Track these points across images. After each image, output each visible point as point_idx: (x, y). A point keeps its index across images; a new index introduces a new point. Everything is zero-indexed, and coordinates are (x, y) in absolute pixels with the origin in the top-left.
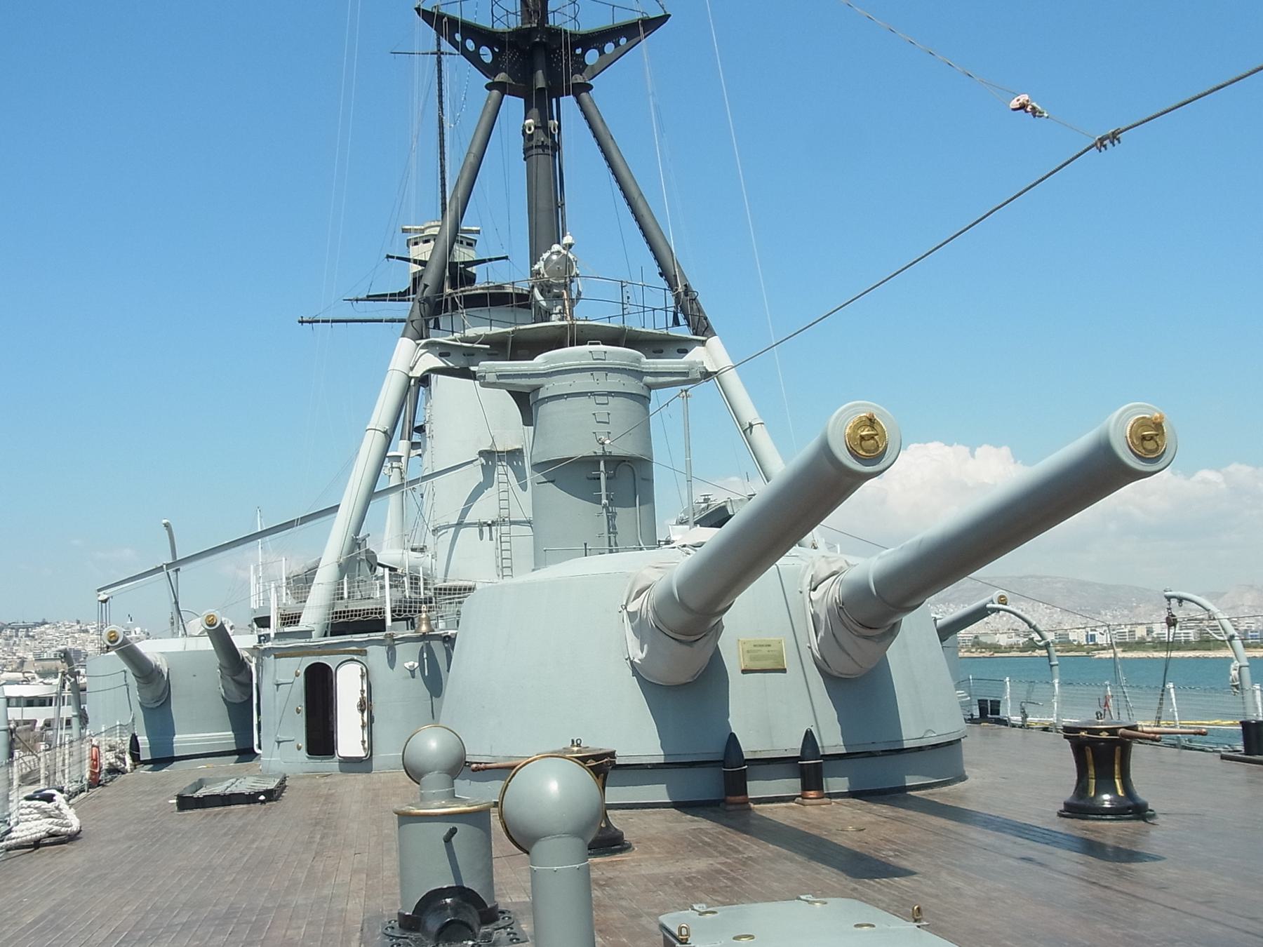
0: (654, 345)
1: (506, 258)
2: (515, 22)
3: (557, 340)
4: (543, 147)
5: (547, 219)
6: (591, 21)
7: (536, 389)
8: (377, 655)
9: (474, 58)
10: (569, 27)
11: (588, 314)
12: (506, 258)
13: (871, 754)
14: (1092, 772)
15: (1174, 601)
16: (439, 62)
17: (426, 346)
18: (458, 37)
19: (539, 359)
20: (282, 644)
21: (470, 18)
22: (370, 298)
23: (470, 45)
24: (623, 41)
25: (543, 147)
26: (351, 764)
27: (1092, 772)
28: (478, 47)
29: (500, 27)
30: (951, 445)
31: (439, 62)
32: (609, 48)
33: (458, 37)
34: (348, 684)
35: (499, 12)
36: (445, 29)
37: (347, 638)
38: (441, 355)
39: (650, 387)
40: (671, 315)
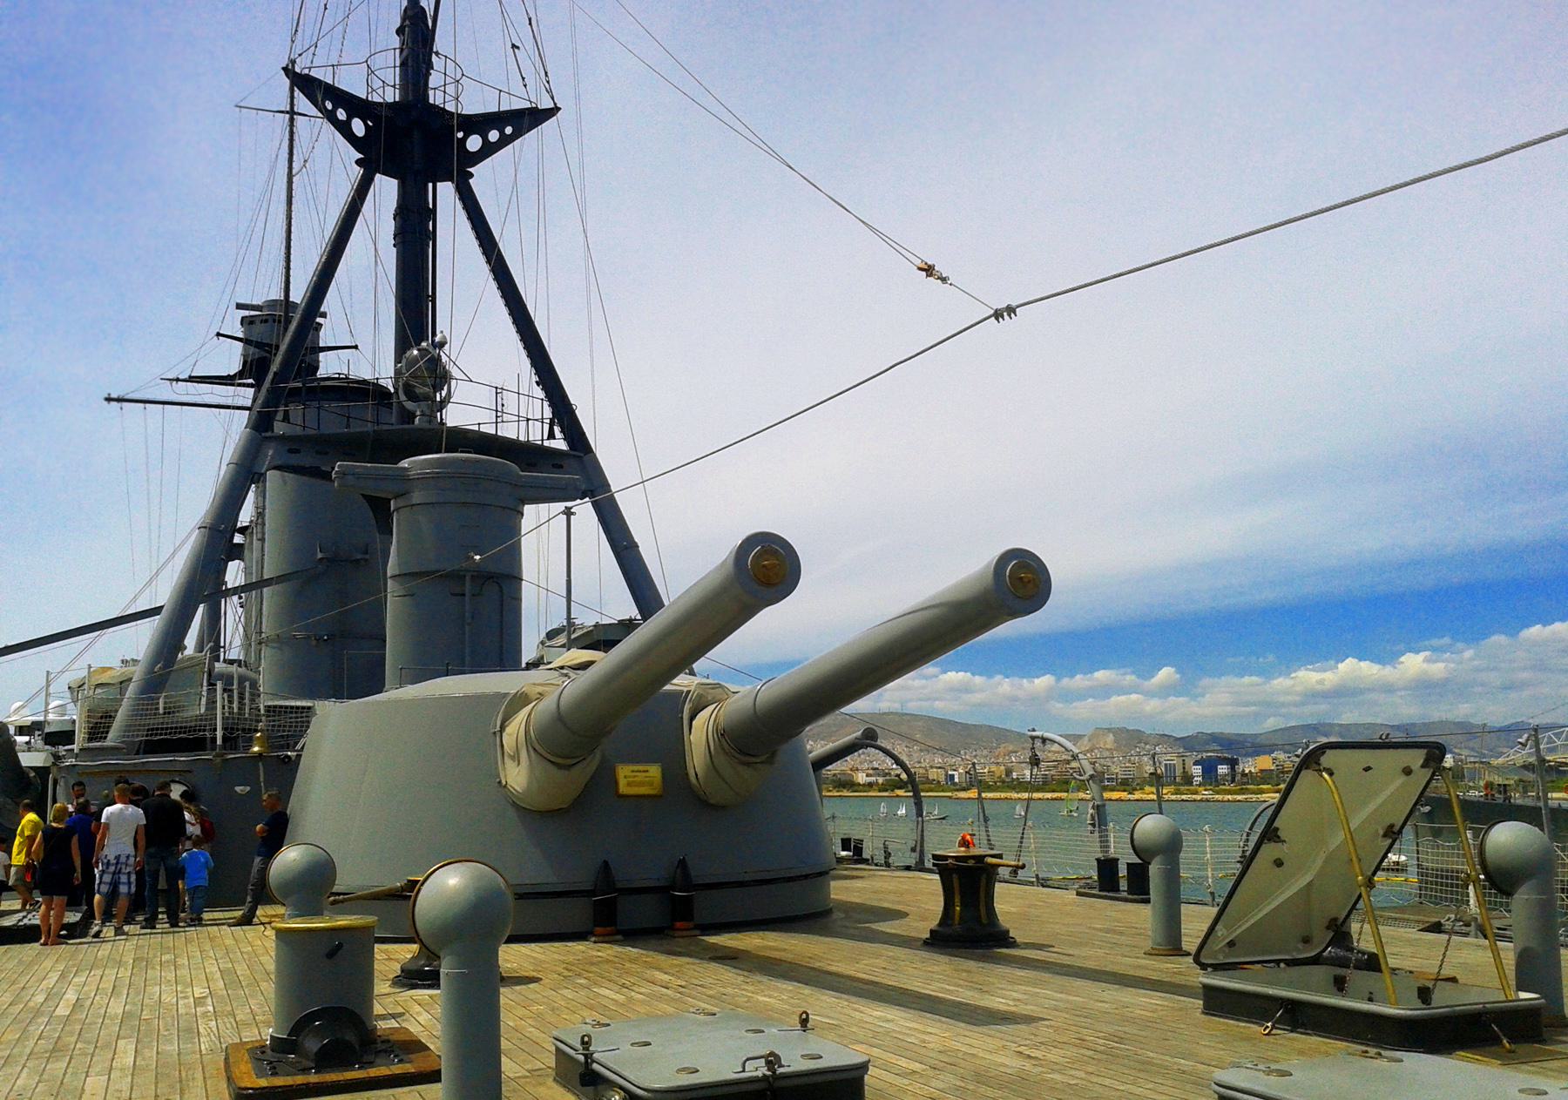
1: (356, 347)
2: (392, 95)
6: (473, 104)
9: (344, 129)
10: (450, 107)
12: (356, 347)
13: (741, 884)
14: (957, 900)
15: (1038, 744)
16: (292, 120)
18: (329, 106)
22: (192, 379)
23: (341, 115)
24: (509, 130)
27: (957, 900)
28: (350, 118)
30: (1262, 771)
31: (292, 120)
32: (494, 136)
35: (377, 84)
40: (546, 427)
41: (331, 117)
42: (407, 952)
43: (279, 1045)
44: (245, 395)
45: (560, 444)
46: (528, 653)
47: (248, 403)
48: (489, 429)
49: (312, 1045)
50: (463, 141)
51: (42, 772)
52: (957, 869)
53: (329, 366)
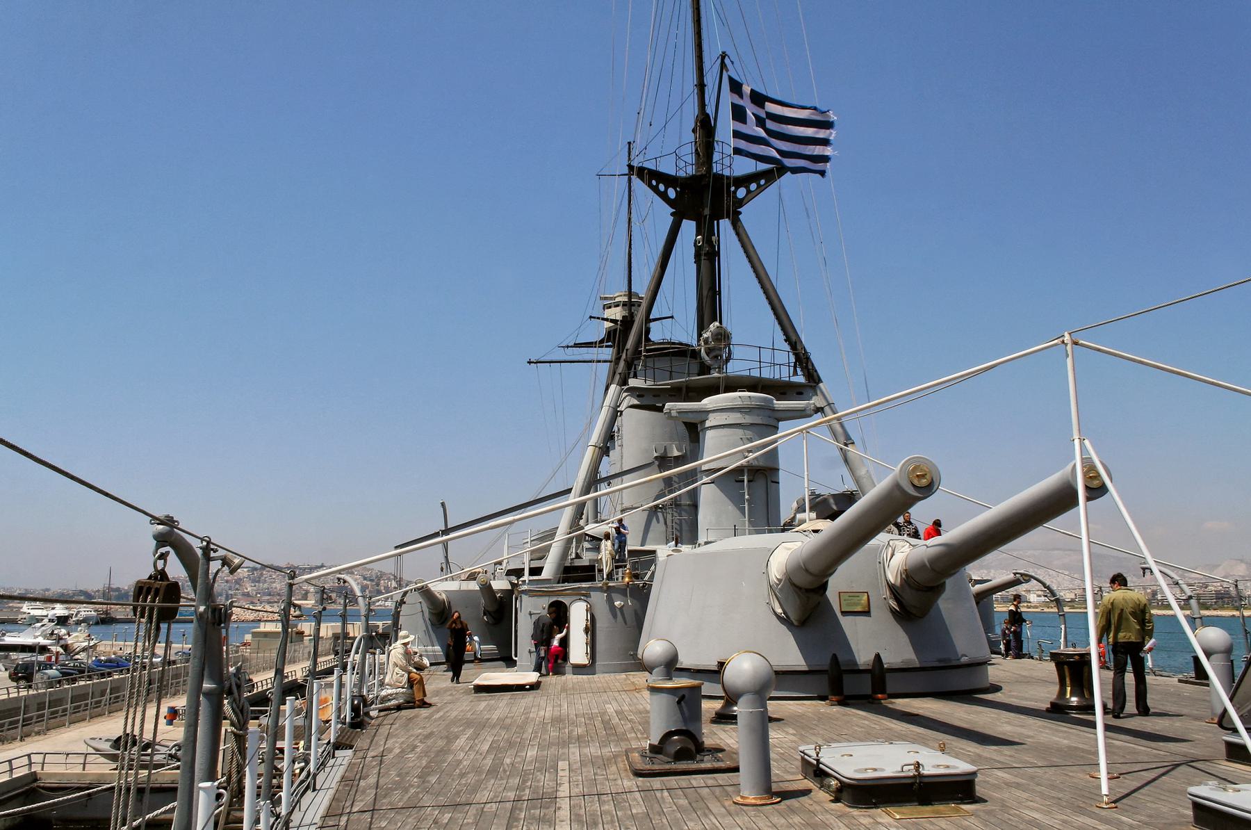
0: (781, 389)
2: (691, 171)
3: (713, 389)
4: (708, 256)
5: (709, 304)
7: (703, 422)
8: (599, 598)
9: (664, 196)
10: (726, 172)
11: (735, 368)
17: (627, 391)
18: (654, 183)
19: (705, 401)
20: (532, 587)
21: (662, 169)
22: (577, 345)
23: (662, 187)
25: (708, 256)
26: (579, 669)
29: (682, 174)
32: (753, 187)
33: (654, 183)
34: (578, 614)
36: (646, 177)
37: (577, 585)
38: (639, 396)
39: (779, 420)
41: (655, 189)
42: (718, 705)
43: (655, 750)
44: (608, 353)
45: (800, 379)
46: (785, 517)
47: (609, 358)
48: (755, 373)
49: (672, 749)
50: (735, 192)
51: (509, 593)
52: (1069, 664)
53: (657, 333)
